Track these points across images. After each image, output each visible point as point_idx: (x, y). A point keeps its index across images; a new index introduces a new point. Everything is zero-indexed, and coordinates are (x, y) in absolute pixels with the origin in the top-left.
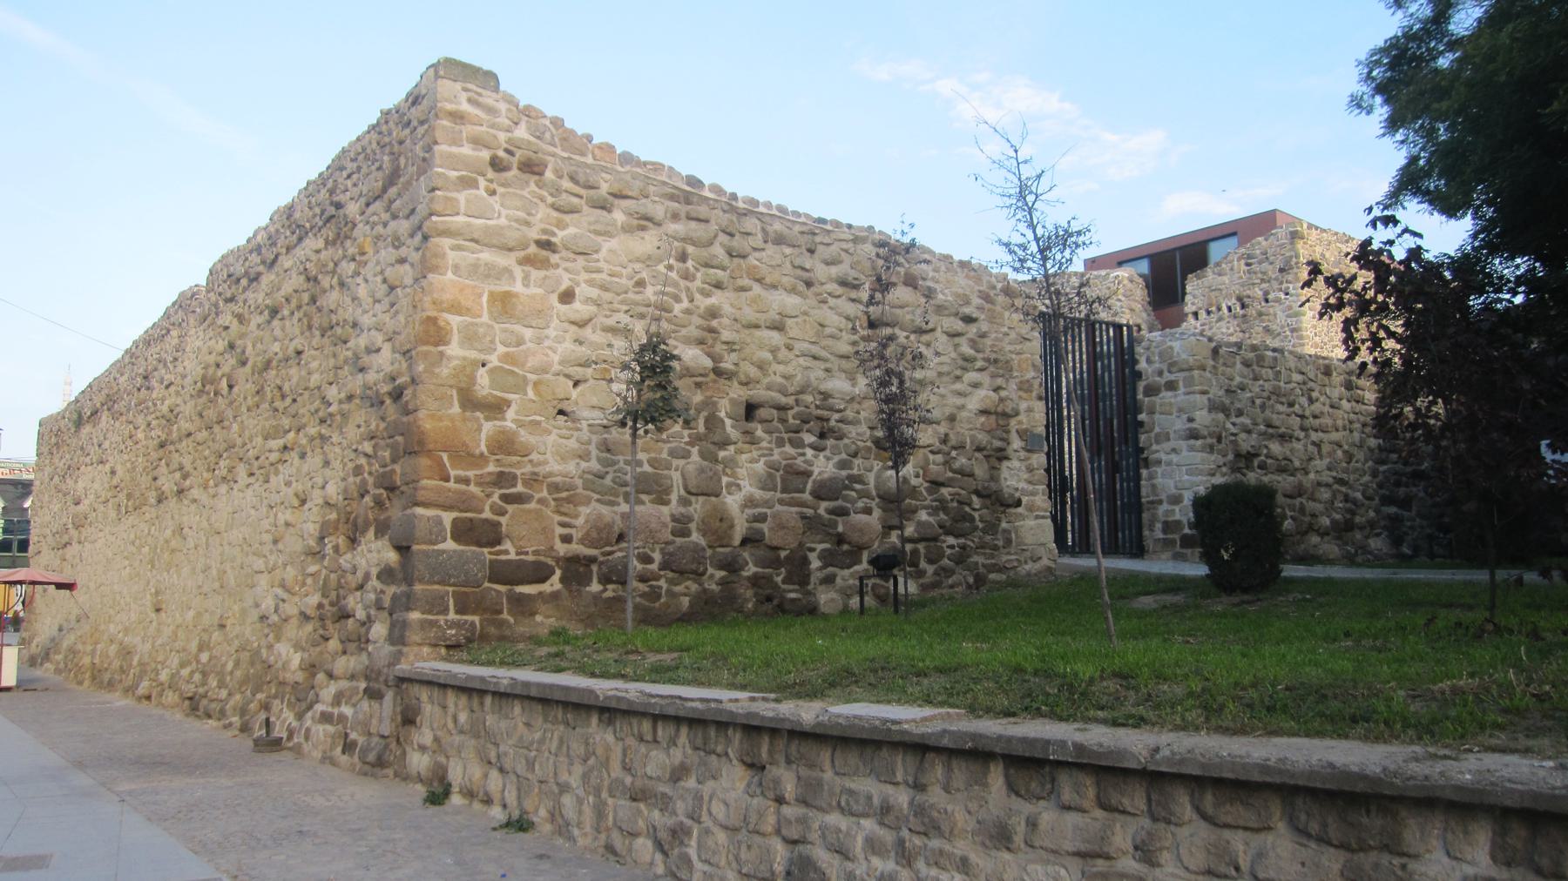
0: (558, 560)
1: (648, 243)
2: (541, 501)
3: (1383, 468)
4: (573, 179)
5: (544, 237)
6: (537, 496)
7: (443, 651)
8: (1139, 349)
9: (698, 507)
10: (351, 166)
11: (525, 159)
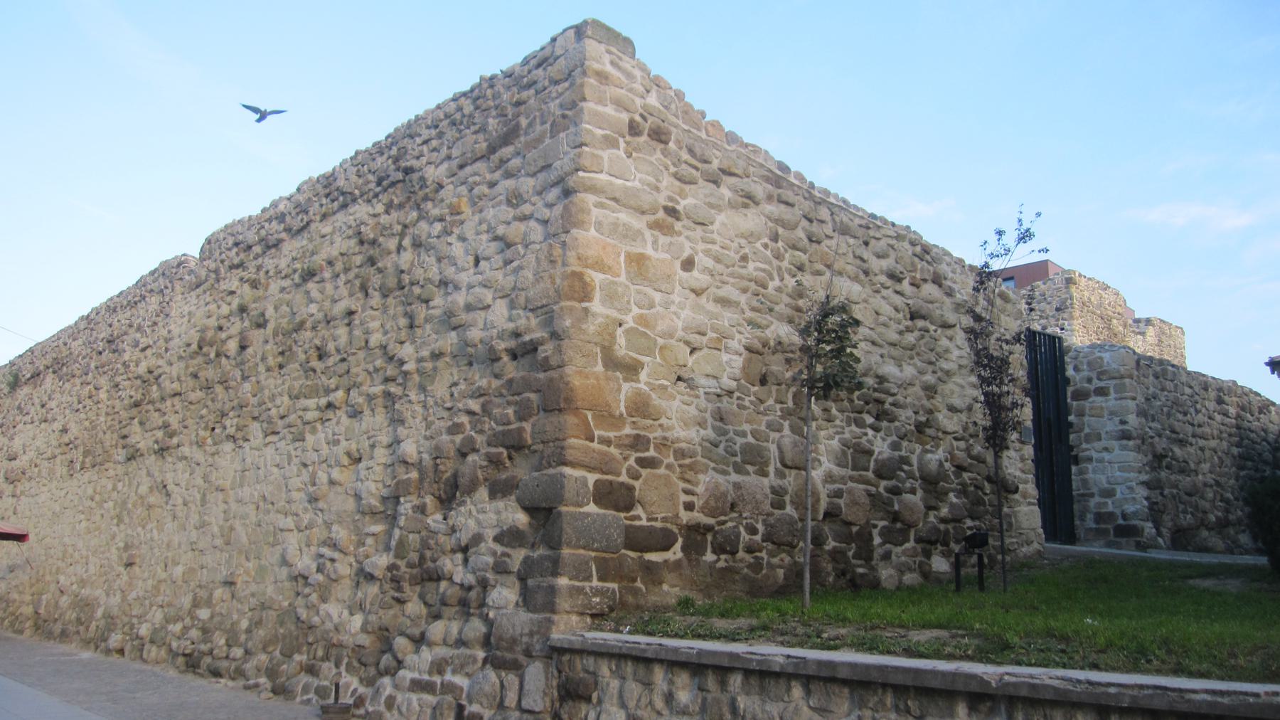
0: (681, 527)
1: (752, 220)
2: (669, 467)
3: (1242, 473)
4: (691, 151)
5: (670, 204)
6: (666, 461)
7: (589, 620)
8: (1067, 359)
9: (791, 481)
10: (426, 133)
11: (659, 127)
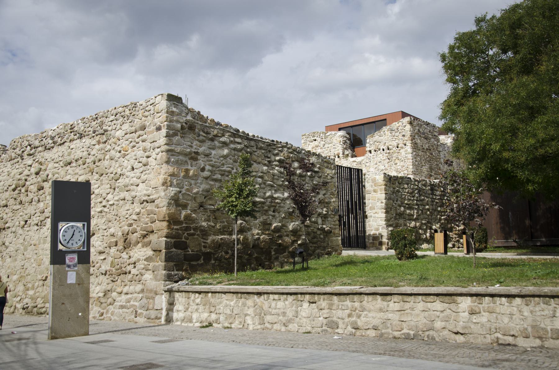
2: (198, 235)
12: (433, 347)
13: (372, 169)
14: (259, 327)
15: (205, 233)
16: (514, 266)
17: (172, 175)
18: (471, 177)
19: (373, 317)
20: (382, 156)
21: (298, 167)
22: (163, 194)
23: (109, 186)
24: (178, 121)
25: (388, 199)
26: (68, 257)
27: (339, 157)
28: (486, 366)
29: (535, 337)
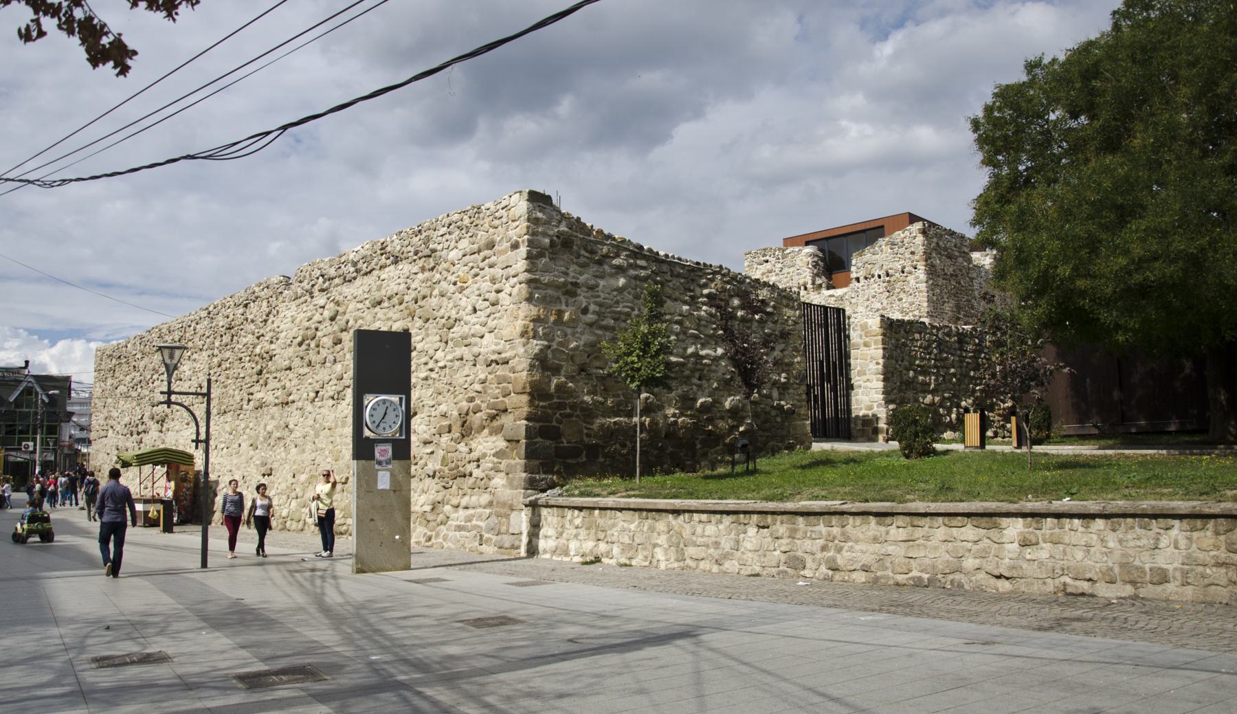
12: (960, 599)
13: (860, 309)
14: (676, 565)
15: (588, 413)
16: (1094, 467)
17: (537, 320)
18: (1025, 320)
19: (862, 552)
20: (876, 287)
21: (741, 308)
22: (521, 350)
23: (438, 338)
24: (545, 234)
25: (889, 356)
26: (378, 449)
27: (806, 289)
28: (1046, 630)
29: (1125, 582)
